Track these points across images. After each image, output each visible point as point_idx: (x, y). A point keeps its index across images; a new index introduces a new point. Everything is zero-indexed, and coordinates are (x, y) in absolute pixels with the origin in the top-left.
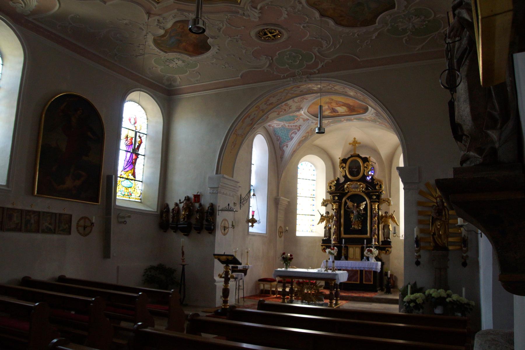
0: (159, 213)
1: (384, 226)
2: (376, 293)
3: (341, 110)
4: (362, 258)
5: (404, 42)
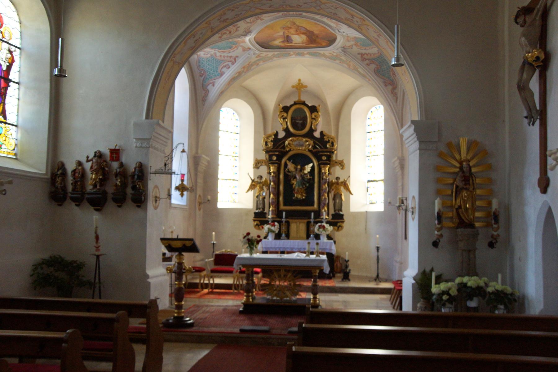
0: (49, 176)
1: (335, 196)
2: (332, 280)
3: (298, 39)
4: (308, 237)
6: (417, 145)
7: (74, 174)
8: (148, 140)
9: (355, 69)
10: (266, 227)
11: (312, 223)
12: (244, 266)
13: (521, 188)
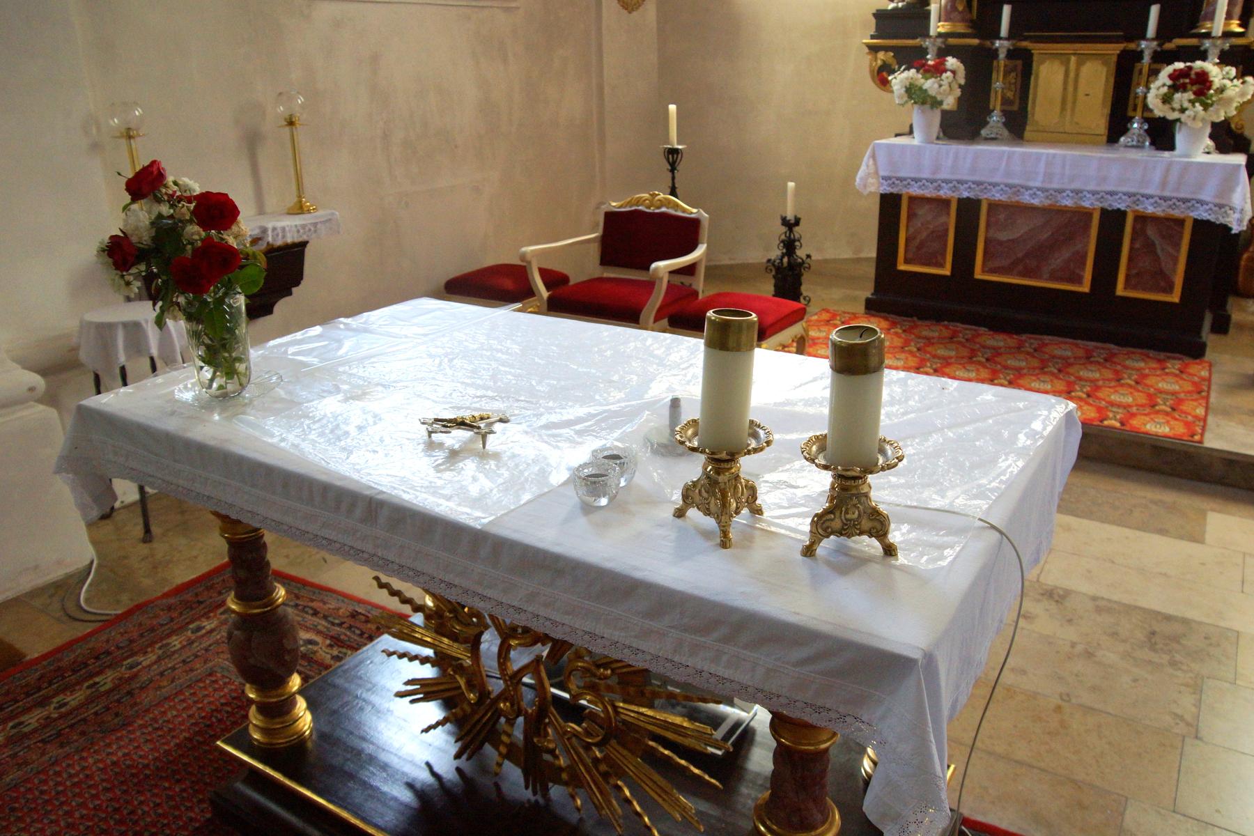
11: (1147, 59)
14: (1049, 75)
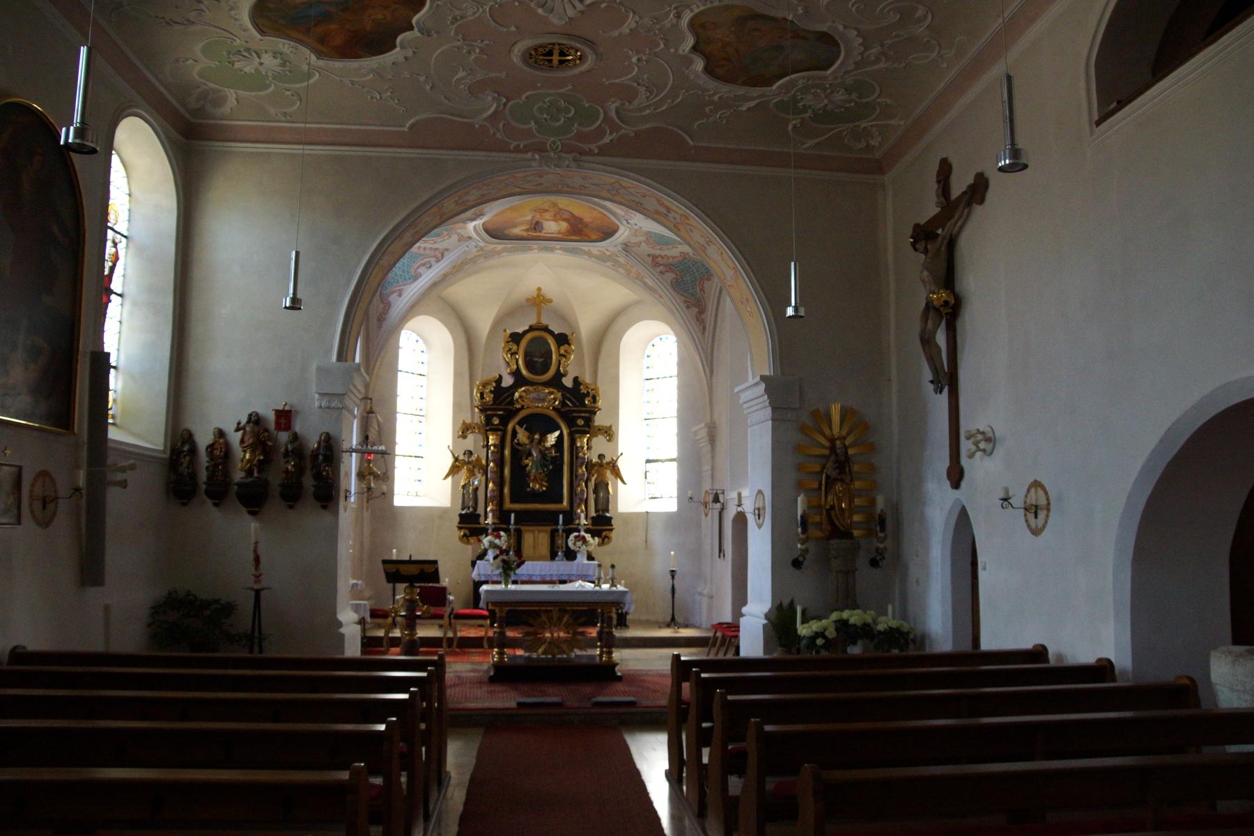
0: (167, 456)
3: (552, 227)
5: (790, 127)
6: (768, 412)
7: (211, 452)
8: (341, 396)
9: (639, 278)
10: (486, 541)
12: (495, 604)
13: (918, 481)
14: (528, 538)
